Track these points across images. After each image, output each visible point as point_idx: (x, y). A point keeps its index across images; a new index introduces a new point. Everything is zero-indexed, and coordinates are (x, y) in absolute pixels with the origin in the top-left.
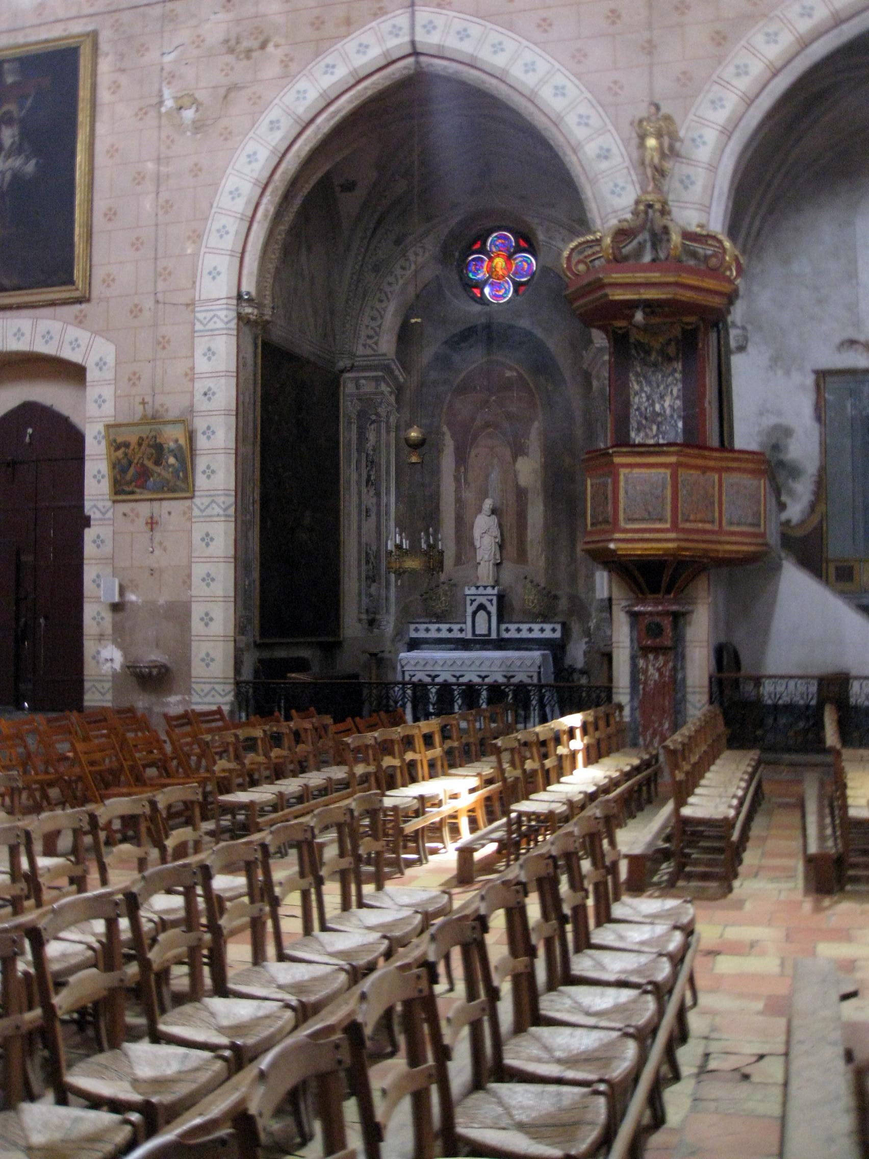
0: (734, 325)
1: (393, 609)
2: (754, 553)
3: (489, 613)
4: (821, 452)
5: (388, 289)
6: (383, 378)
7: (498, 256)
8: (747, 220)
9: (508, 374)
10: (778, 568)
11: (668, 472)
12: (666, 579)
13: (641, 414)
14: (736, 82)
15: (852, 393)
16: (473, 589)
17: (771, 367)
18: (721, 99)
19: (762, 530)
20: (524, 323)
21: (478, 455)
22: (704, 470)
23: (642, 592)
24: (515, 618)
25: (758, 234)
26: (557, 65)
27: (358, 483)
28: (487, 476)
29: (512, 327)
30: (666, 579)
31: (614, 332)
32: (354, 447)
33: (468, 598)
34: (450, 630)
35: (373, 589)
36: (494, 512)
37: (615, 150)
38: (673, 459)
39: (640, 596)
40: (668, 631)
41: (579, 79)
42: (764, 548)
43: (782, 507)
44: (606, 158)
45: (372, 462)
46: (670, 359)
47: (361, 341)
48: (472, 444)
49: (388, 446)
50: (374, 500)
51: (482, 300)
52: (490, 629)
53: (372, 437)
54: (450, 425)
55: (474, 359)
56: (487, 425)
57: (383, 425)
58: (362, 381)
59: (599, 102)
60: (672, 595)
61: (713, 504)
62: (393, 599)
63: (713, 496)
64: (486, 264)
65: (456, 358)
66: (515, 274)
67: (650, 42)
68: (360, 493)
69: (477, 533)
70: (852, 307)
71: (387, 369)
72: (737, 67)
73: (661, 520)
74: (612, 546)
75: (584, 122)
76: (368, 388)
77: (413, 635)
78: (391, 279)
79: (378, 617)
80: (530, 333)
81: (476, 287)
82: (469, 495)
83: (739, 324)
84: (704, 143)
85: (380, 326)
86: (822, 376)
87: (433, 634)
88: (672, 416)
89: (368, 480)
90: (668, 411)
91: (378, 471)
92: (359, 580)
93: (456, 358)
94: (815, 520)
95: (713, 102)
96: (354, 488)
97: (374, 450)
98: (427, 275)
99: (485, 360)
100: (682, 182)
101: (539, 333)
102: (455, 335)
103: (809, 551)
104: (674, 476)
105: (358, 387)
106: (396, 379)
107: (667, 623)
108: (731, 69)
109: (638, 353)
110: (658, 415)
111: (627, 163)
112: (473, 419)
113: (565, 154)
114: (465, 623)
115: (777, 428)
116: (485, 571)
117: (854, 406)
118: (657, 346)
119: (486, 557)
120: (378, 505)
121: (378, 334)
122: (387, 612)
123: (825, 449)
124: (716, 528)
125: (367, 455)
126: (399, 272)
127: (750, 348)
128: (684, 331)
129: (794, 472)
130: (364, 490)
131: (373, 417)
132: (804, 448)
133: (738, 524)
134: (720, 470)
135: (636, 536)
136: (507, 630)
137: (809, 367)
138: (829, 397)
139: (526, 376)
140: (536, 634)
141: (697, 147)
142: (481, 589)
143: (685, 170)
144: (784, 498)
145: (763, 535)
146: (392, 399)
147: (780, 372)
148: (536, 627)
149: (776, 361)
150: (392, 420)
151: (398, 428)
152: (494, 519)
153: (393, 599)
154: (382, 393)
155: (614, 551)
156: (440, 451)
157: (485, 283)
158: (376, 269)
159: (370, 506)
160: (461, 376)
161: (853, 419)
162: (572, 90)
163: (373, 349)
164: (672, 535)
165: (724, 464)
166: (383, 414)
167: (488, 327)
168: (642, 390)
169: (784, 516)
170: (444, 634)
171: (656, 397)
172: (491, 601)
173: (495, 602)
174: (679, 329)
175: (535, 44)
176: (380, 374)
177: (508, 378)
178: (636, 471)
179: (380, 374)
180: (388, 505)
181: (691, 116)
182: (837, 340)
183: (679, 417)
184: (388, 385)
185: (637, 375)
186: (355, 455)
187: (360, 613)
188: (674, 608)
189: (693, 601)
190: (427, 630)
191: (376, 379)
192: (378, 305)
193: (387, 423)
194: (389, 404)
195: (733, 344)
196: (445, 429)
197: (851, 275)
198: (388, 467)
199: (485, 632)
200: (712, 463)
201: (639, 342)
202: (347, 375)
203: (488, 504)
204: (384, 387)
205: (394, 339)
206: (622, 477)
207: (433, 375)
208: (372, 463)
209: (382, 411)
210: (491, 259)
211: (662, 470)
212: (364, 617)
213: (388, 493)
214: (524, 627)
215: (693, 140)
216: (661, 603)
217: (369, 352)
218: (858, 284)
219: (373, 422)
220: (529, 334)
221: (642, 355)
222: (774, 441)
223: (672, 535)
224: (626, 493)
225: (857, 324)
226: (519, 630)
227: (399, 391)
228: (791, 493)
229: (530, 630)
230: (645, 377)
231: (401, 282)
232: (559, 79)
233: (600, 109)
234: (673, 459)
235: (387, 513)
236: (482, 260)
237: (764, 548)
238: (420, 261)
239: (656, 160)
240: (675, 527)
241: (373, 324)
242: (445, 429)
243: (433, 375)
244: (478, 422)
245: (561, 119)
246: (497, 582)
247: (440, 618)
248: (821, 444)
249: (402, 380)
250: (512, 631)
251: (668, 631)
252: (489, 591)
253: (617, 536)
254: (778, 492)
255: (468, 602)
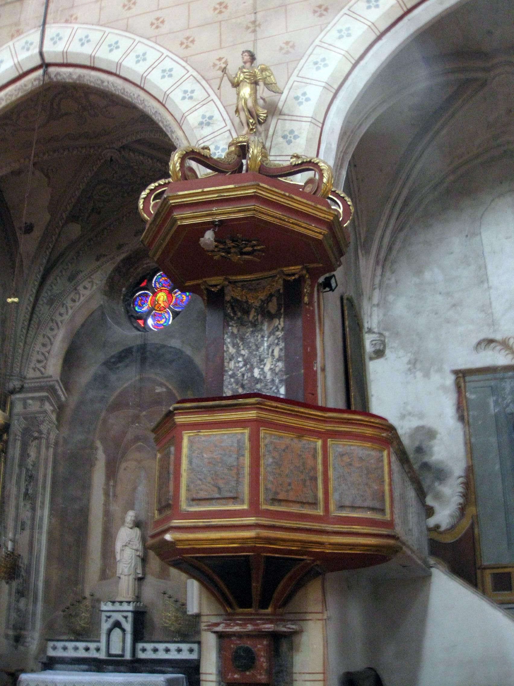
0: (370, 331)
1: (39, 624)
2: (377, 547)
3: (124, 630)
4: (466, 451)
5: (59, 319)
6: (47, 398)
7: (161, 291)
8: (379, 233)
9: (158, 390)
10: (425, 578)
11: (247, 431)
12: (256, 586)
13: (237, 383)
14: (338, 43)
15: (494, 391)
16: (110, 604)
17: (409, 369)
18: (324, 60)
19: (388, 517)
20: (175, 343)
21: (127, 468)
22: (301, 432)
23: (231, 606)
24: (155, 638)
25: (390, 249)
26: (166, 53)
27: (17, 497)
28: (135, 489)
29: (164, 346)
30: (256, 586)
31: (209, 292)
32: (17, 461)
33: (104, 615)
34: (87, 649)
35: (22, 604)
36: (137, 524)
37: (217, 116)
38: (252, 414)
39: (229, 610)
40: (263, 661)
41: (186, 62)
42: (391, 542)
43: (430, 512)
44: (208, 124)
45: (31, 477)
46: (271, 317)
47: (32, 365)
48: (122, 457)
49: (46, 460)
50: (29, 514)
51: (146, 329)
52: (123, 649)
53: (32, 452)
54: (104, 440)
55: (128, 377)
56: (137, 439)
57: (44, 441)
58: (30, 402)
59: (204, 78)
60: (269, 610)
61: (315, 479)
62: (39, 616)
63: (315, 468)
64: (150, 297)
65: (113, 377)
66: (175, 305)
67: (254, 22)
68: (17, 508)
69: (118, 545)
70: (486, 308)
71: (52, 390)
72: (340, 31)
73: (235, 499)
74: (168, 537)
75: (188, 96)
76: (34, 407)
77: (51, 653)
78: (63, 310)
79: (23, 632)
80: (181, 352)
81: (140, 318)
82: (115, 508)
83: (376, 330)
84: (308, 100)
85: (49, 352)
86: (462, 375)
87: (71, 654)
88: (273, 381)
89: (26, 494)
90: (269, 376)
91: (36, 485)
92: (10, 595)
93: (113, 377)
94: (466, 524)
95: (316, 63)
96: (12, 502)
97: (33, 466)
98: (94, 305)
99: (138, 378)
100: (284, 137)
101: (188, 351)
102: (113, 357)
103: (462, 558)
104: (255, 440)
105: (25, 406)
106: (58, 397)
107: (260, 648)
108: (334, 33)
109: (235, 314)
110: (258, 381)
111: (229, 126)
112: (124, 433)
113: (172, 132)
114: (99, 641)
115: (420, 429)
116: (125, 586)
117: (496, 403)
118: (257, 304)
119: (126, 570)
120: (33, 519)
121: (46, 359)
122: (33, 628)
123: (470, 449)
124: (320, 512)
125: (27, 470)
126: (69, 304)
127: (387, 352)
128: (286, 283)
129: (440, 474)
130: (22, 504)
131: (36, 434)
132: (449, 448)
133: (353, 508)
134: (324, 435)
135: (200, 522)
136: (144, 650)
137: (447, 368)
138: (471, 396)
139: (175, 391)
140: (173, 655)
141: (300, 103)
142: (117, 604)
143: (289, 125)
144: (430, 501)
145: (390, 524)
146: (54, 417)
147: (419, 374)
148: (173, 647)
149: (414, 364)
150: (52, 437)
151: (56, 444)
152: (137, 532)
153: (39, 616)
154: (45, 412)
155: (172, 544)
156: (92, 465)
157: (149, 313)
158: (51, 302)
159: (26, 520)
160: (116, 393)
161: (496, 415)
162: (179, 71)
163: (42, 373)
164: (251, 520)
165: (329, 427)
166: (45, 431)
167: (143, 348)
168: (238, 352)
169: (432, 522)
170: (82, 654)
171: (255, 361)
172: (126, 617)
173: (130, 619)
174: (281, 281)
175: (148, 39)
176: (45, 394)
177: (159, 394)
178: (204, 433)
179: (45, 394)
180: (41, 519)
181: (294, 78)
182: (475, 341)
183: (281, 381)
184: (52, 405)
185: (233, 336)
186: (16, 470)
187: (7, 627)
188: (269, 627)
189: (300, 617)
190: (65, 648)
191: (42, 400)
192: (50, 334)
193: (47, 439)
194: (51, 422)
195: (369, 348)
196: (98, 444)
197: (482, 280)
198: (45, 482)
199: (119, 652)
200: (311, 425)
201: (237, 301)
202: (18, 396)
203: (130, 516)
204: (48, 407)
205: (60, 362)
206: (185, 442)
207: (92, 394)
208: (31, 478)
209: (44, 428)
210: (155, 294)
211: (238, 430)
212: (11, 633)
213: (42, 508)
214: (161, 646)
215: (297, 98)
216: (251, 621)
217: (38, 374)
218: (489, 288)
219: (36, 438)
220: (179, 353)
221: (239, 314)
222: (417, 444)
223: (251, 520)
224: (190, 462)
225: (493, 324)
226: (155, 650)
227: (61, 408)
228: (438, 496)
229: (167, 650)
230: (242, 339)
231: (70, 312)
232: (168, 64)
233: (204, 83)
234: (252, 414)
235: (40, 527)
236: (147, 296)
237: (391, 542)
238: (86, 295)
239: (250, 104)
240: (254, 509)
241: (44, 350)
242: (98, 444)
243: (92, 394)
244: (129, 436)
245: (167, 96)
246: (138, 598)
247: (80, 635)
248: (466, 444)
249: (63, 398)
250: (148, 651)
251: (263, 661)
252: (125, 607)
253: (176, 522)
254: (421, 494)
255: (104, 618)
